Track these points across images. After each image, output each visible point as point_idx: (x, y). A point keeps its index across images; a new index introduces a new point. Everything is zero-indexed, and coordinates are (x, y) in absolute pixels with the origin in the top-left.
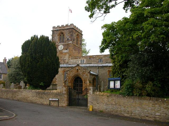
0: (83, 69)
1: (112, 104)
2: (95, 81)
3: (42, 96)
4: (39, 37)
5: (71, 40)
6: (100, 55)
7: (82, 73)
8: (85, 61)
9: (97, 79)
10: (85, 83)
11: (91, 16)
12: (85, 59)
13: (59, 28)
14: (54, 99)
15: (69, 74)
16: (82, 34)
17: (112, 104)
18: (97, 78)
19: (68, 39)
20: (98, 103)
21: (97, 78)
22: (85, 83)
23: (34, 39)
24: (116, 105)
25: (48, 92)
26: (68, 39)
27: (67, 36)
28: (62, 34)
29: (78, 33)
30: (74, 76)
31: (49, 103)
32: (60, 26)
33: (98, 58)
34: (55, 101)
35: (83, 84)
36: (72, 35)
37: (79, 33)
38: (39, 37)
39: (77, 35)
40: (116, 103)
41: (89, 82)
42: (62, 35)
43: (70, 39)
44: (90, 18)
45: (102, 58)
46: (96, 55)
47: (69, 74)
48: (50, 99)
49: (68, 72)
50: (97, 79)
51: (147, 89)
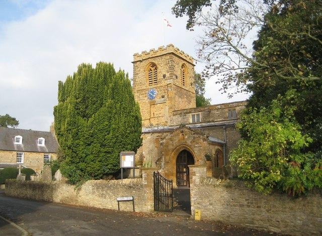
1: (241, 206)
3: (104, 192)
4: (94, 67)
5: (171, 77)
6: (230, 103)
8: (201, 117)
9: (224, 152)
12: (200, 113)
14: (125, 199)
17: (241, 206)
18: (224, 150)
19: (164, 76)
20: (211, 204)
21: (224, 150)
23: (84, 69)
24: (249, 206)
25: (114, 184)
26: (164, 76)
27: (162, 70)
29: (185, 62)
30: (176, 148)
31: (117, 207)
34: (128, 201)
36: (172, 68)
37: (186, 61)
38: (94, 67)
39: (183, 66)
40: (248, 203)
42: (152, 69)
43: (168, 75)
44: (177, 17)
45: (235, 110)
48: (119, 199)
50: (224, 152)
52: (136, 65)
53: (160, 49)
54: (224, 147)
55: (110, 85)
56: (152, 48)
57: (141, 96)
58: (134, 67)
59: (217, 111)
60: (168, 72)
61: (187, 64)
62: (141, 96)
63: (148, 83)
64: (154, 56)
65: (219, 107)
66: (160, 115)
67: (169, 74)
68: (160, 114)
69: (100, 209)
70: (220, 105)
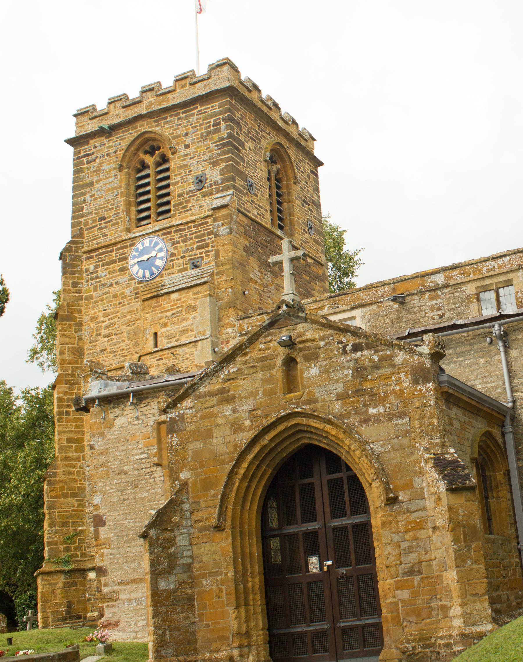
0: (356, 348)
2: (500, 476)
7: (341, 397)
10: (392, 501)
11: (345, 231)
13: (187, 339)
15: (196, 435)
16: (317, 153)
18: (510, 438)
19: (200, 181)
22: (392, 501)
26: (200, 181)
28: (151, 152)
32: (134, 94)
33: (471, 289)
35: (376, 521)
41: (442, 486)
42: (150, 160)
46: (454, 267)
47: (196, 435)
49: (188, 403)
51: (394, 650)
52: (84, 149)
53: (180, 79)
54: (509, 428)
55: (21, 440)
56: (149, 81)
57: (102, 272)
58: (78, 160)
59: (431, 298)
60: (215, 164)
61: (292, 152)
62: (102, 272)
63: (134, 216)
64: (155, 108)
65: (440, 279)
66: (184, 340)
67: (218, 168)
68: (184, 332)
69: (380, 604)
70: (444, 270)
